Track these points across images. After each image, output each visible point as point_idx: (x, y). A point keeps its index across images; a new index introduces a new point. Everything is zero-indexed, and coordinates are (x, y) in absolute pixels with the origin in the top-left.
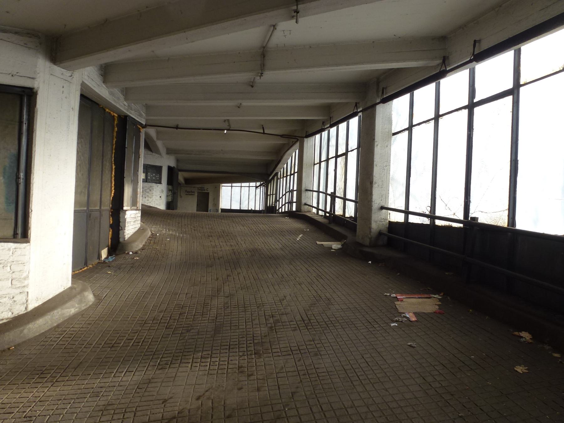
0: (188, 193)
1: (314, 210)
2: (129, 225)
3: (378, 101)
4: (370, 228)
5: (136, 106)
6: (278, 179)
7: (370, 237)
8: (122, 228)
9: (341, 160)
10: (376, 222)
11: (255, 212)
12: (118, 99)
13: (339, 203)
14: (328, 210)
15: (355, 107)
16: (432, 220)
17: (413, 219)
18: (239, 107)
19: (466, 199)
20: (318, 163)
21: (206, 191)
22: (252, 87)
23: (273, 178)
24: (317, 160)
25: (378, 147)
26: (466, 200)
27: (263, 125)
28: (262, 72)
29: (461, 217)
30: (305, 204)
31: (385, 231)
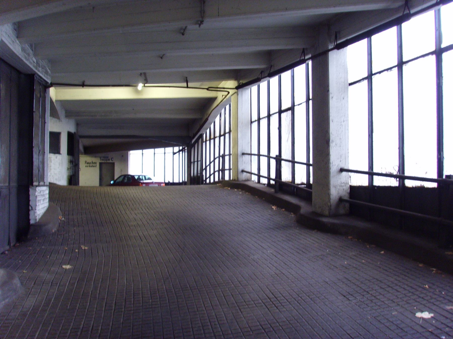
0: (89, 165)
1: (254, 178)
2: (39, 204)
3: (330, 47)
4: (329, 195)
5: (43, 62)
6: (202, 142)
7: (330, 205)
8: (32, 207)
9: (286, 117)
10: (335, 187)
11: (173, 184)
12: (29, 55)
13: (286, 168)
14: (273, 176)
15: (302, 54)
16: (401, 180)
17: (379, 182)
18: (161, 58)
19: (439, 155)
20: (256, 121)
21: (110, 161)
22: (183, 34)
23: (197, 141)
24: (255, 117)
25: (334, 99)
26: (439, 156)
27: (187, 78)
28: (202, 19)
29: (435, 176)
30: (243, 171)
31: (346, 197)
